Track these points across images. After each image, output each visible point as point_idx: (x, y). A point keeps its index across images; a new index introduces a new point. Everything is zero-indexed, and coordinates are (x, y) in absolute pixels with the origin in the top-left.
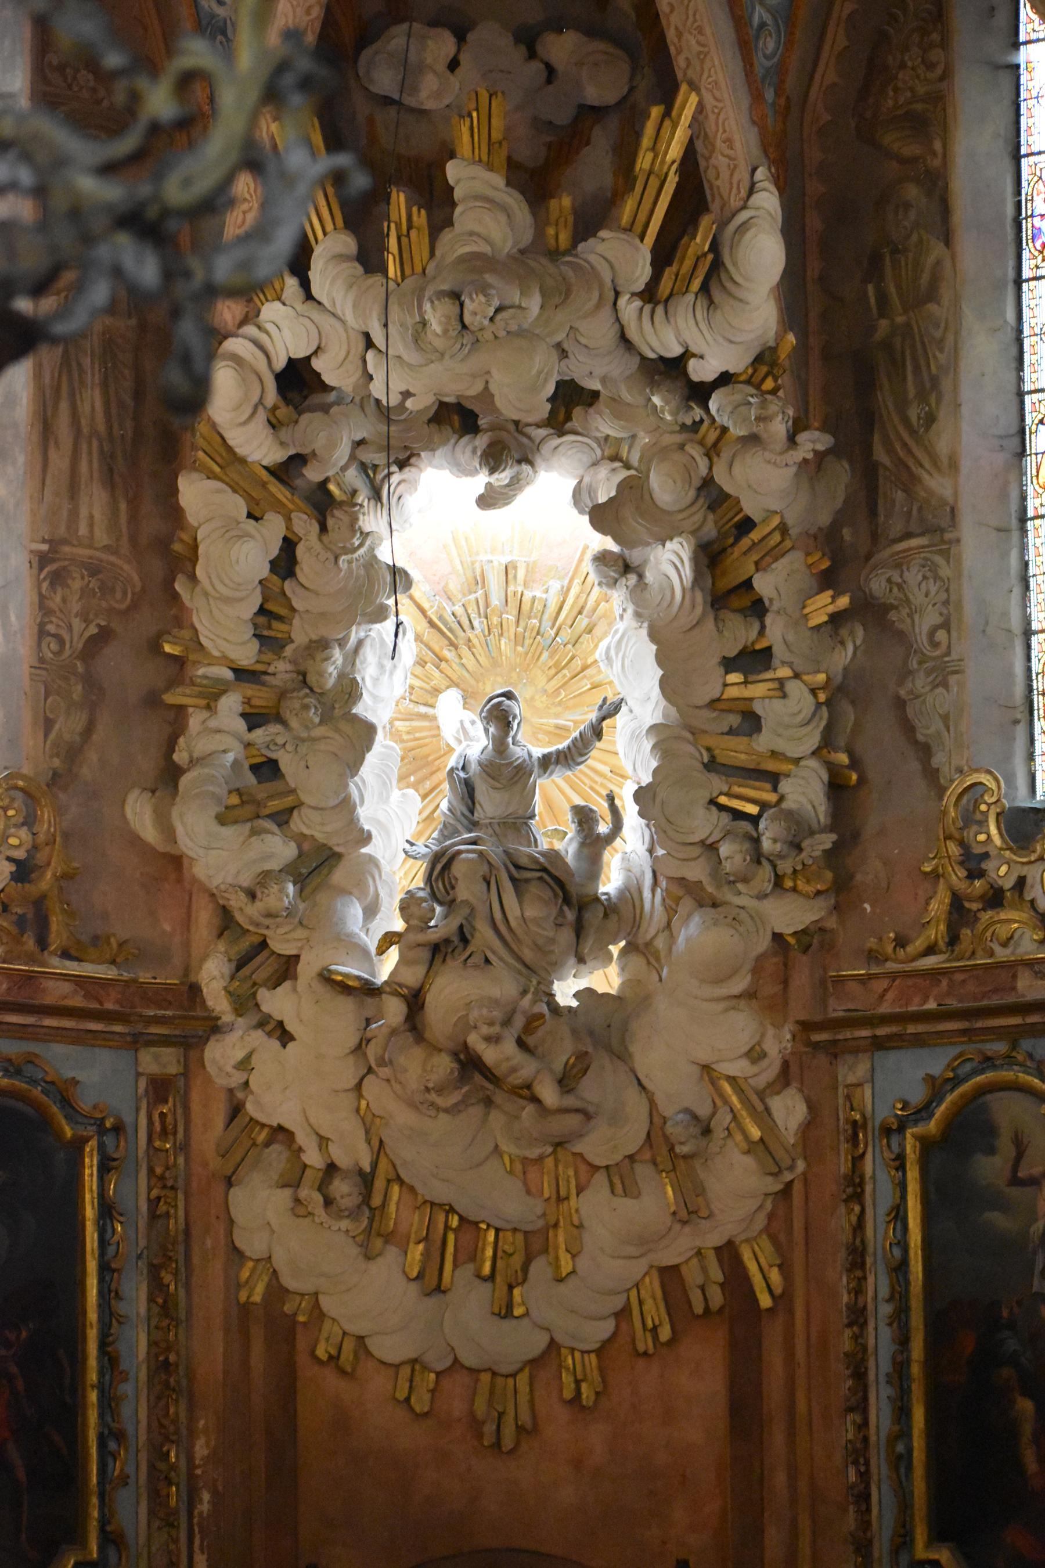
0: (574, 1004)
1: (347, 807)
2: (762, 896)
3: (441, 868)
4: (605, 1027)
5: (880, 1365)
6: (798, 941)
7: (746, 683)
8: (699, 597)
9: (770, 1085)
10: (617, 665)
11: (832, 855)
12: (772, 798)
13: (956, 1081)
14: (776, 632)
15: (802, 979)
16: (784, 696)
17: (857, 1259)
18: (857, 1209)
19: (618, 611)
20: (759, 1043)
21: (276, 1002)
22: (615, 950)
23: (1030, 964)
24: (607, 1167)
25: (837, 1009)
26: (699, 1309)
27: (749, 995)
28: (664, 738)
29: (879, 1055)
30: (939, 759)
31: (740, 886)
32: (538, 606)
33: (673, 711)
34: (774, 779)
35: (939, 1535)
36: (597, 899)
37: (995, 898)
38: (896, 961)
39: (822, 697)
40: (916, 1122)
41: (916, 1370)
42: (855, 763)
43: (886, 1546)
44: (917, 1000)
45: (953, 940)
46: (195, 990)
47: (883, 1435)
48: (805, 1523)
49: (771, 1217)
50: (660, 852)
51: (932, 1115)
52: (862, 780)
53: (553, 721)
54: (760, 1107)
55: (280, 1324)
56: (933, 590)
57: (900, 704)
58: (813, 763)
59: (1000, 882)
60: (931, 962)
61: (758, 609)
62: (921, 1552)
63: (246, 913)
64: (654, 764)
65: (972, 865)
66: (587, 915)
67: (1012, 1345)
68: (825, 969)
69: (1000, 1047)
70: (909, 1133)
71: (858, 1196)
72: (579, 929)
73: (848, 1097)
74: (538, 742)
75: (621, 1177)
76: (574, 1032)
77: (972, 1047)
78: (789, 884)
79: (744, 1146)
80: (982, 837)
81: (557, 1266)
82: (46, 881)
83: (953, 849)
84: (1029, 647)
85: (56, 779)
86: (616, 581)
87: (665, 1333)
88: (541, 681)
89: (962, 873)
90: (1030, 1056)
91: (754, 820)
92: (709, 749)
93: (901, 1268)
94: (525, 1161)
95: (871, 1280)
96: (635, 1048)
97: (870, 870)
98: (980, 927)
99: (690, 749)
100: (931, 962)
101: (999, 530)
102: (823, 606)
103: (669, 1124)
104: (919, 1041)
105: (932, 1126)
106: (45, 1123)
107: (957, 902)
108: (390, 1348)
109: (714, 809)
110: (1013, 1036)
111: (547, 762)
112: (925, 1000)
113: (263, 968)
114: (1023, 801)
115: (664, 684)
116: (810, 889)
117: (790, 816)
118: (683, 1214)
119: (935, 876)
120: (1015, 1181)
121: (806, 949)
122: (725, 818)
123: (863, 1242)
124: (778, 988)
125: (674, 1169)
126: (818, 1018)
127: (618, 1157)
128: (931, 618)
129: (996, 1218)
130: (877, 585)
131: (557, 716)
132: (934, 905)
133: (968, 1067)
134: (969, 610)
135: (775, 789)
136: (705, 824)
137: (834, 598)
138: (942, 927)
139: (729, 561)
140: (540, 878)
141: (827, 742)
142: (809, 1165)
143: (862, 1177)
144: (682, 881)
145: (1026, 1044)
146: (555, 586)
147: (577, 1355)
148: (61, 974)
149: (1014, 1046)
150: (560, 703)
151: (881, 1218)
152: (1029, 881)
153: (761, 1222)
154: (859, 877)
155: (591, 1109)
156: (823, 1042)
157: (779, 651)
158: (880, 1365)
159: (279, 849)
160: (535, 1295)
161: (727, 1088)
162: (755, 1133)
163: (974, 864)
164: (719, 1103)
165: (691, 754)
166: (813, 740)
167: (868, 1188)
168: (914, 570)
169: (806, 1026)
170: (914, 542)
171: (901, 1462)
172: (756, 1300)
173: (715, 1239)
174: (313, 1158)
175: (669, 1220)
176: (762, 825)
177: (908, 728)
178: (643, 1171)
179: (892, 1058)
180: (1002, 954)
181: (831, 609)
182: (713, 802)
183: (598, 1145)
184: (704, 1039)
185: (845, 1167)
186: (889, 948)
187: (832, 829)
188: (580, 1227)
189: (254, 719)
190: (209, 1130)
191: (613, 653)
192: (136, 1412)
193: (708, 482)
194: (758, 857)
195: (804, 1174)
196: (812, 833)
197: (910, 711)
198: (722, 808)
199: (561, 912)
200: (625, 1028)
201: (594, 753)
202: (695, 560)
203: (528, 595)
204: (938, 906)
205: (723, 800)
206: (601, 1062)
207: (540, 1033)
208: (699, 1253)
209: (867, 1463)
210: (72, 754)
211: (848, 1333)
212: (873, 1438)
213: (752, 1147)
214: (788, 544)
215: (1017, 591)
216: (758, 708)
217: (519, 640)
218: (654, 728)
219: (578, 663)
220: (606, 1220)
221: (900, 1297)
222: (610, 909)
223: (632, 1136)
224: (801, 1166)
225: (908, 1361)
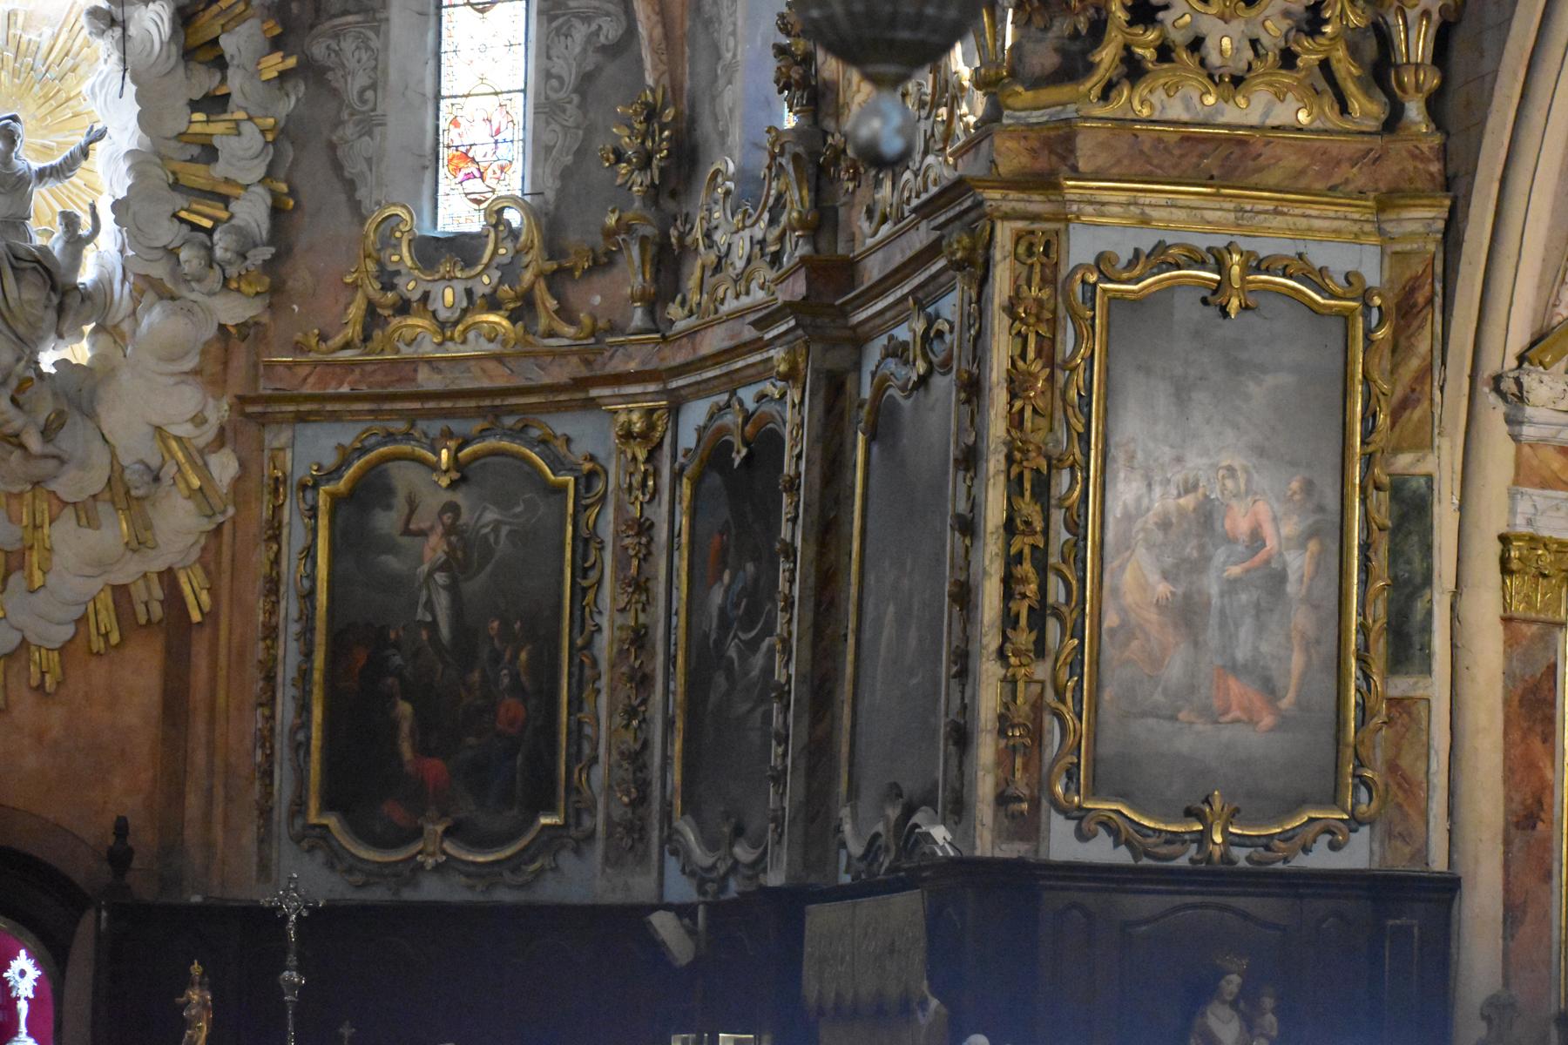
0: (53, 371)
2: (211, 294)
4: (79, 393)
5: (287, 671)
6: (239, 332)
7: (208, 121)
8: (174, 49)
9: (208, 445)
10: (100, 99)
11: (269, 266)
12: (224, 215)
13: (363, 451)
14: (235, 82)
15: (240, 360)
16: (239, 134)
17: (273, 586)
18: (275, 547)
19: (103, 56)
20: (201, 411)
22: (88, 328)
23: (429, 362)
24: (75, 504)
25: (265, 388)
26: (143, 620)
27: (196, 372)
28: (138, 162)
29: (299, 426)
30: (361, 194)
31: (194, 284)
32: (33, 48)
33: (147, 141)
34: (225, 200)
35: (328, 805)
36: (76, 288)
37: (403, 308)
38: (317, 352)
39: (270, 137)
40: (328, 481)
41: (317, 676)
42: (292, 192)
43: (284, 815)
44: (334, 384)
45: (367, 338)
47: (286, 730)
48: (219, 792)
49: (204, 549)
50: (130, 253)
51: (341, 477)
52: (297, 205)
53: (40, 141)
54: (200, 462)
56: (365, 57)
57: (332, 147)
58: (260, 190)
59: (409, 295)
60: (347, 355)
61: (220, 63)
62: (313, 818)
64: (129, 182)
65: (385, 279)
66: (68, 301)
67: (397, 660)
68: (258, 355)
69: (400, 426)
70: (322, 489)
71: (276, 538)
72: (61, 310)
73: (273, 459)
74: (37, 159)
75: (85, 513)
76: (55, 394)
77: (377, 424)
78: (234, 285)
79: (186, 493)
80: (395, 258)
81: (31, 581)
83: (371, 266)
84: (438, 109)
86: (103, 32)
87: (115, 638)
88: (32, 107)
89: (377, 286)
90: (426, 435)
91: (209, 232)
92: (174, 173)
93: (310, 595)
94: (9, 495)
95: (283, 604)
96: (102, 411)
97: (300, 277)
98: (390, 329)
99: (160, 172)
100: (347, 355)
101: (420, 14)
102: (274, 64)
103: (127, 472)
104: (335, 417)
105: (342, 485)
107: (371, 309)
109: (176, 222)
110: (412, 417)
111: (42, 175)
112: (341, 384)
114: (428, 232)
115: (142, 119)
116: (252, 290)
117: (240, 232)
118: (134, 544)
119: (355, 286)
120: (407, 532)
121: (244, 338)
122: (185, 229)
123: (278, 574)
124: (219, 368)
125: (129, 508)
126: (252, 394)
127: (84, 496)
128: (361, 80)
129: (392, 562)
130: (318, 50)
131: (43, 137)
132: (352, 311)
133: (373, 440)
134: (393, 76)
135: (227, 208)
136: (168, 233)
137: (284, 58)
138: (358, 328)
139: (198, 24)
140: (34, 269)
141: (270, 174)
142: (237, 510)
143: (280, 523)
144: (146, 277)
145: (422, 425)
146: (48, 32)
147: (43, 652)
149: (413, 426)
150: (46, 127)
151: (294, 556)
152: (432, 296)
153: (195, 553)
154: (290, 283)
155: (66, 457)
156: (254, 415)
157: (236, 98)
158: (287, 671)
161: (174, 445)
162: (196, 483)
163: (388, 280)
164: (167, 456)
165: (160, 176)
166: (260, 172)
167: (285, 532)
168: (350, 40)
169: (242, 400)
170: (350, 18)
171: (301, 748)
172: (188, 616)
173: (159, 565)
175: (122, 548)
176: (216, 237)
177: (337, 166)
178: (103, 508)
179: (309, 430)
180: (406, 352)
181: (281, 67)
182: (175, 215)
183: (68, 485)
184: (158, 405)
185: (266, 513)
186: (313, 341)
187: (270, 242)
188: (50, 550)
191: (97, 90)
194: (211, 262)
195: (233, 518)
196: (255, 246)
197: (340, 153)
198: (182, 221)
199: (49, 298)
200: (93, 392)
201: (78, 171)
202: (173, 21)
203: (25, 38)
204: (356, 311)
205: (183, 214)
206: (74, 418)
207: (28, 393)
208: (145, 575)
209: (272, 747)
211: (261, 645)
212: (278, 729)
213: (193, 494)
214: (250, 11)
215: (431, 63)
216: (216, 142)
217: (15, 73)
218: (130, 153)
219: (63, 95)
220: (71, 544)
221: (307, 618)
222: (86, 296)
223: (96, 480)
224: (231, 511)
225: (311, 669)
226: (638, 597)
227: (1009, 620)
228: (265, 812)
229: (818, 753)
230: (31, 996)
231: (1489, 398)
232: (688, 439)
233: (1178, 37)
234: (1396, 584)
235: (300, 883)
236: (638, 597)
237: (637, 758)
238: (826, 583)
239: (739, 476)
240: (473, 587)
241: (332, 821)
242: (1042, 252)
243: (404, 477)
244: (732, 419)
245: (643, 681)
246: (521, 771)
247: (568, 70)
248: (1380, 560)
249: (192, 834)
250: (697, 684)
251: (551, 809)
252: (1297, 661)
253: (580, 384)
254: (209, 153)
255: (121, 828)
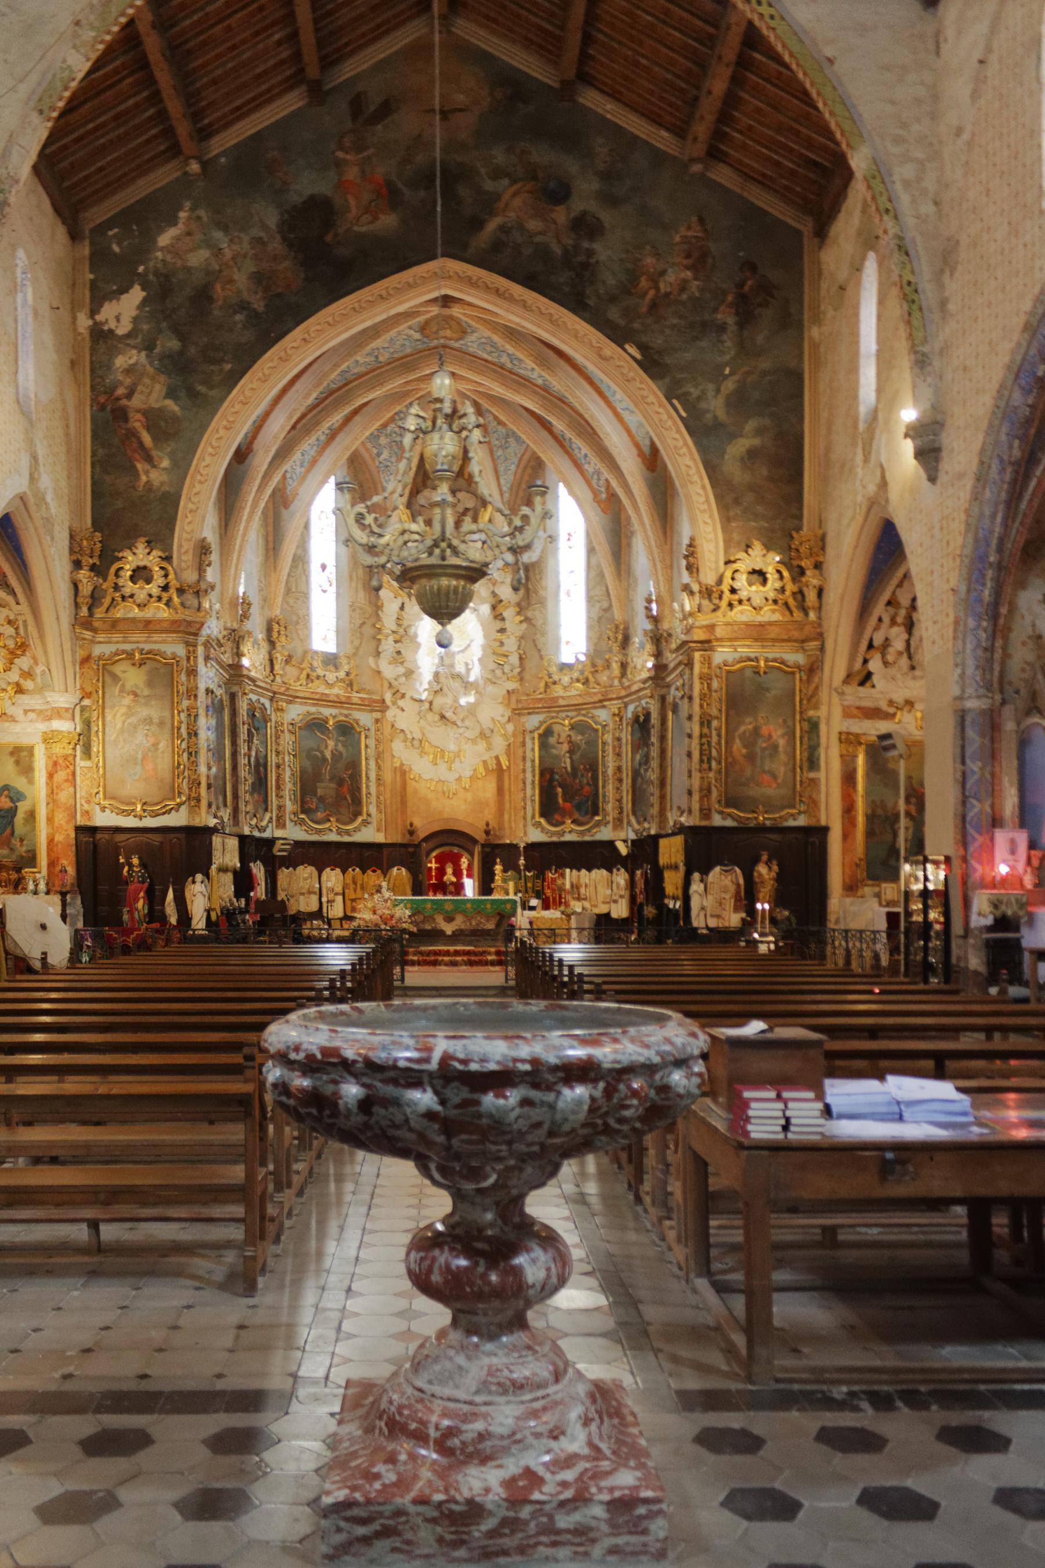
1: (415, 661)
3: (436, 675)
5: (529, 781)
11: (520, 673)
17: (524, 759)
21: (401, 703)
37: (555, 683)
46: (383, 701)
55: (402, 772)
61: (503, 619)
63: (395, 683)
82: (352, 676)
85: (355, 654)
93: (533, 761)
97: (527, 676)
105: (541, 731)
106: (353, 728)
108: (425, 776)
113: (399, 695)
129: (554, 751)
130: (529, 614)
136: (493, 666)
148: (356, 697)
156: (518, 712)
158: (529, 781)
159: (401, 670)
160: (456, 765)
174: (409, 736)
189: (396, 642)
190: (387, 730)
192: (373, 790)
193: (493, 592)
204: (542, 684)
210: (357, 649)
221: (533, 767)
222: (472, 684)
226: (615, 760)
227: (701, 761)
228: (525, 818)
229: (662, 797)
230: (199, 877)
231: (834, 694)
232: (630, 715)
233: (744, 598)
234: (810, 747)
235: (536, 836)
236: (615, 760)
237: (620, 801)
238: (663, 752)
239: (642, 724)
240: (575, 757)
241: (542, 820)
242: (708, 661)
243: (556, 728)
244: (639, 709)
245: (620, 780)
246: (589, 806)
247: (595, 616)
248: (806, 739)
249: (506, 825)
250: (634, 781)
251: (597, 814)
252: (782, 769)
253: (601, 701)
254: (502, 644)
255: (487, 825)
